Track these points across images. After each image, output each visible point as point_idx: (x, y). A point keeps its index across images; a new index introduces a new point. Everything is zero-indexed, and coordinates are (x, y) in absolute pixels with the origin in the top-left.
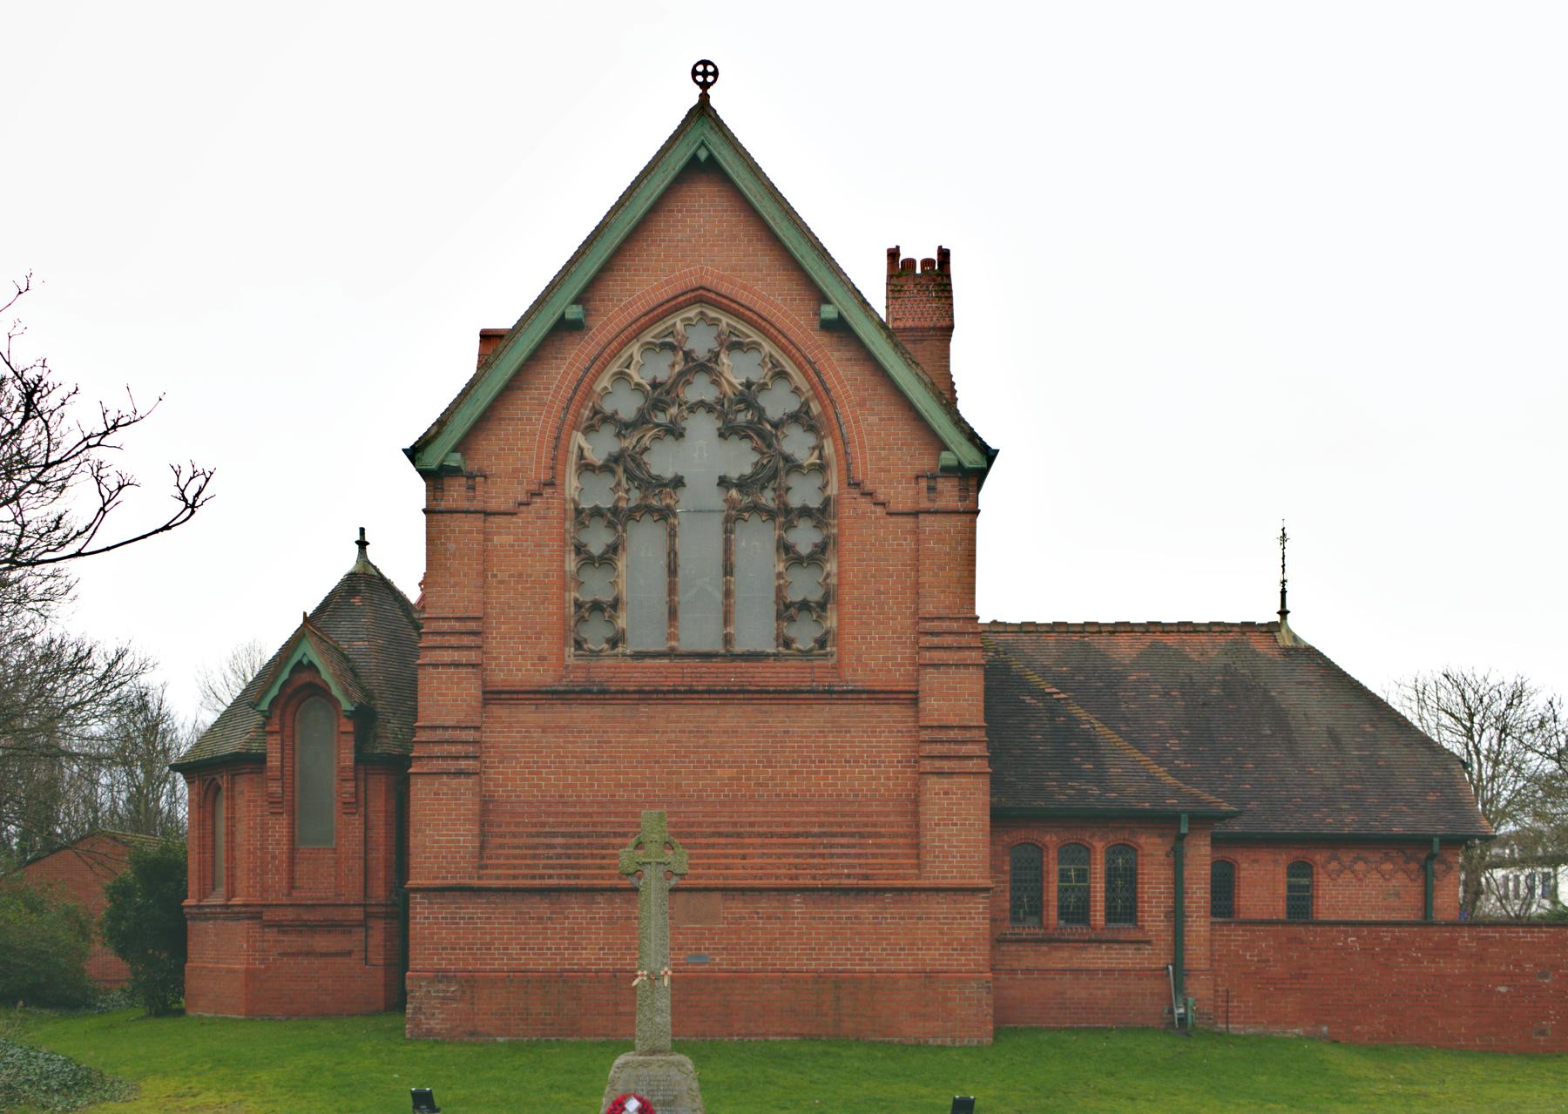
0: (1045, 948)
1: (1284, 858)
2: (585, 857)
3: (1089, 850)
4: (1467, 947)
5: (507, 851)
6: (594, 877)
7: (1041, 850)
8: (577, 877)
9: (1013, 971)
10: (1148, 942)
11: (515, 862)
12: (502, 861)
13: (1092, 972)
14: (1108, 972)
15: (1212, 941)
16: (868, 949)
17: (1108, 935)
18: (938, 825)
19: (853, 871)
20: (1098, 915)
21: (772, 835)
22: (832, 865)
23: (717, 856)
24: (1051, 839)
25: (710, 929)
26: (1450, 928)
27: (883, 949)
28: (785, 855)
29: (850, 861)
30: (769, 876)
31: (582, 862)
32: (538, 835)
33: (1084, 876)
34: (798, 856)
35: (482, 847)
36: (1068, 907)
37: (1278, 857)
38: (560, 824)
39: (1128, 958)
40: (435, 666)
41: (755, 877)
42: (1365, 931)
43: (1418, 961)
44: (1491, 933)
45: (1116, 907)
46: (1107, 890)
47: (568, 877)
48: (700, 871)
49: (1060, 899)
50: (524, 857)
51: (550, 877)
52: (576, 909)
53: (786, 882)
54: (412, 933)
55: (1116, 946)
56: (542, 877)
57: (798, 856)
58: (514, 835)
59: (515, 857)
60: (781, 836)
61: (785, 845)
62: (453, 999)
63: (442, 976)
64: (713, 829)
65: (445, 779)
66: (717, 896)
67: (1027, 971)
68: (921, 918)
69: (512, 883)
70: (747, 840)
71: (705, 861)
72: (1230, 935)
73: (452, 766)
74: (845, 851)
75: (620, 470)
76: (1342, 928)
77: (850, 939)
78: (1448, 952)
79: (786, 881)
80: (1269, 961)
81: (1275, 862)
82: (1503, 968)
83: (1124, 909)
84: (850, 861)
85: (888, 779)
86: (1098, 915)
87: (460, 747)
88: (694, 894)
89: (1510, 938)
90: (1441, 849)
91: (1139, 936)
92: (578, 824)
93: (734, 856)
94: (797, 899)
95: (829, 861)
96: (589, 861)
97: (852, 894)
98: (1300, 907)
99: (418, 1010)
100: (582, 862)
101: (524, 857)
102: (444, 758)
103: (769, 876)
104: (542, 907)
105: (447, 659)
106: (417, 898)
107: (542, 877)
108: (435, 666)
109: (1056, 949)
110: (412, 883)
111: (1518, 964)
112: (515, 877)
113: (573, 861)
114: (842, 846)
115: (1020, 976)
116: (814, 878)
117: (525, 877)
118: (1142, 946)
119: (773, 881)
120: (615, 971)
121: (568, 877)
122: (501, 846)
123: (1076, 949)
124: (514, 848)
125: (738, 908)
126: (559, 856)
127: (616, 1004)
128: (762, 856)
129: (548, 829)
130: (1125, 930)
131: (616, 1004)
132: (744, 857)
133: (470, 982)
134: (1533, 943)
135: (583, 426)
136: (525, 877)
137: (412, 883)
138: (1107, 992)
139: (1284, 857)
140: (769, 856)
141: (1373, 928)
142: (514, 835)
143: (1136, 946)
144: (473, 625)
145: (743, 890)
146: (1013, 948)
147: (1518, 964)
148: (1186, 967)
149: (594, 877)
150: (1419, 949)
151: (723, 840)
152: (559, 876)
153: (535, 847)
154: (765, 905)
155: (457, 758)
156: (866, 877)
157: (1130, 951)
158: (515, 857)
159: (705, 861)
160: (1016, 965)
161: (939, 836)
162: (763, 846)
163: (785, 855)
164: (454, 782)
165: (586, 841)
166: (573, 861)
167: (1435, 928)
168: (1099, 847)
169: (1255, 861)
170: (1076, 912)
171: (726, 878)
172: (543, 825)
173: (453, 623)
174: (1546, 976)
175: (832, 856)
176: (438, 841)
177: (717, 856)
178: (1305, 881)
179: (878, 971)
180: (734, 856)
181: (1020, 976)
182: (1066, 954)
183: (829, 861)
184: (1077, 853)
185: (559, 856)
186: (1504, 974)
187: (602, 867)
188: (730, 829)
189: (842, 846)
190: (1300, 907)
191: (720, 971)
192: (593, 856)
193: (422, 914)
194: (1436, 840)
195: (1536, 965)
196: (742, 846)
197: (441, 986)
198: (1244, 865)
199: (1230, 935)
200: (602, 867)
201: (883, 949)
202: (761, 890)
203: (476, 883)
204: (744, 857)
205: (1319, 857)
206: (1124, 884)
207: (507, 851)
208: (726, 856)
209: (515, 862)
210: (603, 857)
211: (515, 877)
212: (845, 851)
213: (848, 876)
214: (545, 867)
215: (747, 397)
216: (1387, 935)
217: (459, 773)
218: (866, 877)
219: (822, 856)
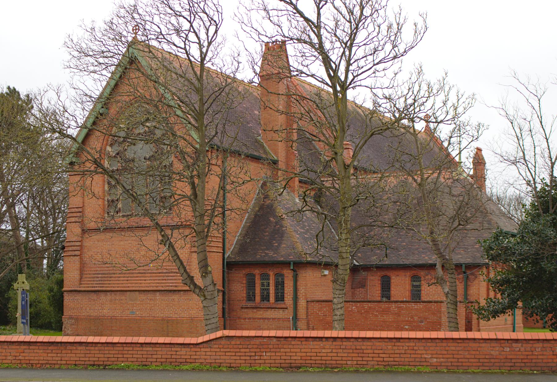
0: (255, 310)
1: (409, 274)
2: (106, 281)
3: (268, 275)
4: (394, 311)
5: (88, 279)
6: (107, 287)
7: (254, 275)
8: (103, 287)
9: (245, 319)
10: (287, 308)
11: (89, 282)
12: (86, 282)
13: (268, 319)
14: (274, 319)
15: (307, 308)
16: (176, 310)
17: (274, 306)
18: (195, 269)
19: (173, 285)
20: (272, 299)
21: (153, 273)
22: (167, 283)
23: (138, 280)
24: (257, 272)
25: (136, 303)
26: (388, 303)
27: (181, 310)
28: (156, 280)
29: (172, 281)
30: (151, 286)
31: (105, 282)
32: (95, 274)
33: (262, 284)
34: (159, 280)
35: (81, 278)
36: (264, 296)
37: (406, 274)
38: (101, 271)
39: (279, 314)
40: (70, 223)
41: (147, 287)
42: (358, 304)
43: (376, 316)
44: (402, 305)
45: (278, 296)
46: (275, 290)
47: (101, 287)
48: (134, 285)
49: (261, 293)
50: (91, 281)
51: (97, 287)
52: (102, 296)
53: (155, 288)
54: (64, 304)
55: (277, 310)
56: (94, 287)
57: (159, 280)
58: (90, 274)
59: (89, 281)
60: (155, 273)
61: (156, 276)
62: (73, 324)
63: (71, 318)
64: (138, 271)
65: (72, 257)
66: (137, 293)
67: (250, 319)
68: (190, 300)
69: (87, 289)
70: (147, 275)
71: (135, 282)
72: (314, 306)
73: (74, 253)
74: (171, 278)
75: (119, 157)
76: (351, 303)
77: (172, 307)
78: (387, 312)
79: (155, 288)
80: (326, 315)
81: (405, 275)
82: (407, 319)
83: (280, 298)
84: (172, 281)
85: (186, 254)
86: (272, 299)
87: (76, 247)
88: (131, 292)
89: (409, 307)
90: (465, 269)
91: (283, 306)
92: (105, 270)
93: (142, 280)
94: (158, 294)
95: (167, 281)
96: (106, 282)
97: (172, 292)
98: (416, 296)
99: (65, 327)
100: (105, 282)
101: (91, 281)
102: (72, 251)
103: (151, 286)
104: (94, 296)
105: (73, 221)
106: (65, 294)
107: (94, 287)
108: (70, 223)
109: (258, 311)
110: (64, 289)
111: (412, 317)
112: (88, 287)
113: (103, 282)
114: (171, 276)
115: (247, 320)
116: (162, 287)
117: (91, 287)
118: (284, 310)
119: (152, 288)
120: (112, 316)
121: (101, 287)
122: (86, 278)
123: (264, 311)
124: (89, 278)
125: (143, 296)
126: (99, 281)
127: (112, 327)
128: (150, 280)
129: (98, 272)
130: (280, 304)
131: (112, 327)
132: (145, 280)
133: (77, 319)
134: (418, 309)
135: (109, 144)
136: (91, 287)
137: (64, 289)
138: (273, 326)
139: (409, 274)
140: (151, 280)
141: (361, 303)
142: (90, 274)
143: (283, 310)
144: (80, 210)
145: (144, 291)
146: (246, 310)
147: (412, 317)
148: (299, 317)
149: (107, 287)
150: (377, 311)
151: (140, 275)
152: (99, 287)
153: (94, 278)
154: (150, 296)
155: (75, 251)
156: (176, 286)
157: (281, 311)
158: (89, 281)
159: (135, 282)
160: (246, 316)
161: (196, 273)
162: (150, 277)
163: (156, 280)
164: (74, 258)
165: (106, 276)
166: (103, 282)
167: (382, 303)
168: (271, 274)
169: (398, 276)
170: (265, 297)
171: (140, 287)
172: (97, 271)
173: (75, 209)
174: (422, 323)
175: (168, 279)
176: (70, 276)
177: (138, 280)
178: (418, 283)
179: (179, 317)
180: (142, 280)
181: (247, 320)
182: (261, 313)
183: (167, 281)
184: (265, 277)
185: (99, 281)
186: (407, 321)
187: (109, 284)
188: (143, 271)
189: (171, 276)
190: (416, 296)
191: (138, 317)
192: (108, 280)
193: (67, 299)
194: (464, 265)
195: (419, 318)
196: (145, 277)
197: (71, 321)
198: (393, 277)
199: (314, 306)
200: (109, 284)
201: (181, 310)
202: (149, 291)
203: (79, 289)
204: (145, 280)
205: (422, 273)
206: (280, 285)
207: (88, 279)
208: (141, 280)
209: (89, 282)
210: (110, 281)
211: (88, 287)
212: (171, 278)
213: (171, 286)
214: (96, 284)
215: (151, 132)
216: (366, 305)
217: (75, 256)
218: (176, 286)
219: (165, 280)
